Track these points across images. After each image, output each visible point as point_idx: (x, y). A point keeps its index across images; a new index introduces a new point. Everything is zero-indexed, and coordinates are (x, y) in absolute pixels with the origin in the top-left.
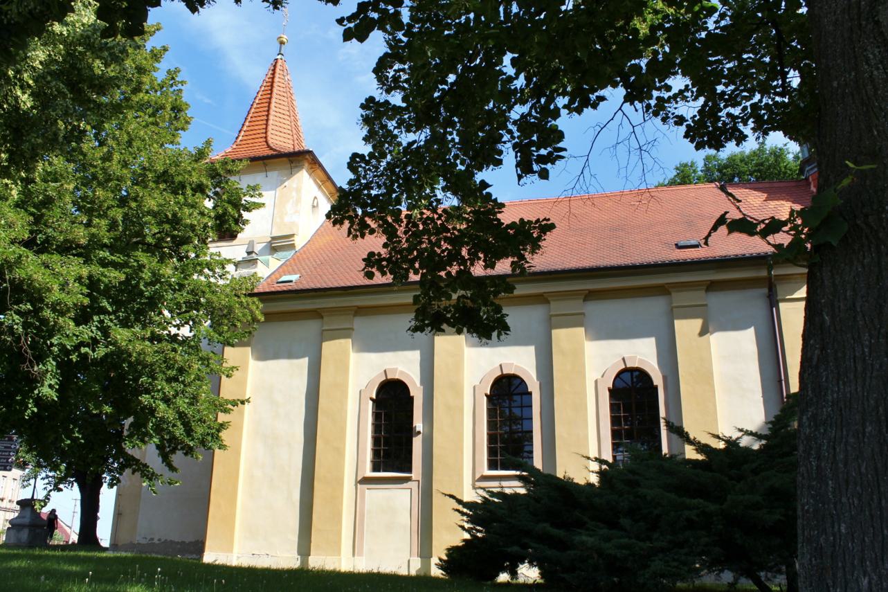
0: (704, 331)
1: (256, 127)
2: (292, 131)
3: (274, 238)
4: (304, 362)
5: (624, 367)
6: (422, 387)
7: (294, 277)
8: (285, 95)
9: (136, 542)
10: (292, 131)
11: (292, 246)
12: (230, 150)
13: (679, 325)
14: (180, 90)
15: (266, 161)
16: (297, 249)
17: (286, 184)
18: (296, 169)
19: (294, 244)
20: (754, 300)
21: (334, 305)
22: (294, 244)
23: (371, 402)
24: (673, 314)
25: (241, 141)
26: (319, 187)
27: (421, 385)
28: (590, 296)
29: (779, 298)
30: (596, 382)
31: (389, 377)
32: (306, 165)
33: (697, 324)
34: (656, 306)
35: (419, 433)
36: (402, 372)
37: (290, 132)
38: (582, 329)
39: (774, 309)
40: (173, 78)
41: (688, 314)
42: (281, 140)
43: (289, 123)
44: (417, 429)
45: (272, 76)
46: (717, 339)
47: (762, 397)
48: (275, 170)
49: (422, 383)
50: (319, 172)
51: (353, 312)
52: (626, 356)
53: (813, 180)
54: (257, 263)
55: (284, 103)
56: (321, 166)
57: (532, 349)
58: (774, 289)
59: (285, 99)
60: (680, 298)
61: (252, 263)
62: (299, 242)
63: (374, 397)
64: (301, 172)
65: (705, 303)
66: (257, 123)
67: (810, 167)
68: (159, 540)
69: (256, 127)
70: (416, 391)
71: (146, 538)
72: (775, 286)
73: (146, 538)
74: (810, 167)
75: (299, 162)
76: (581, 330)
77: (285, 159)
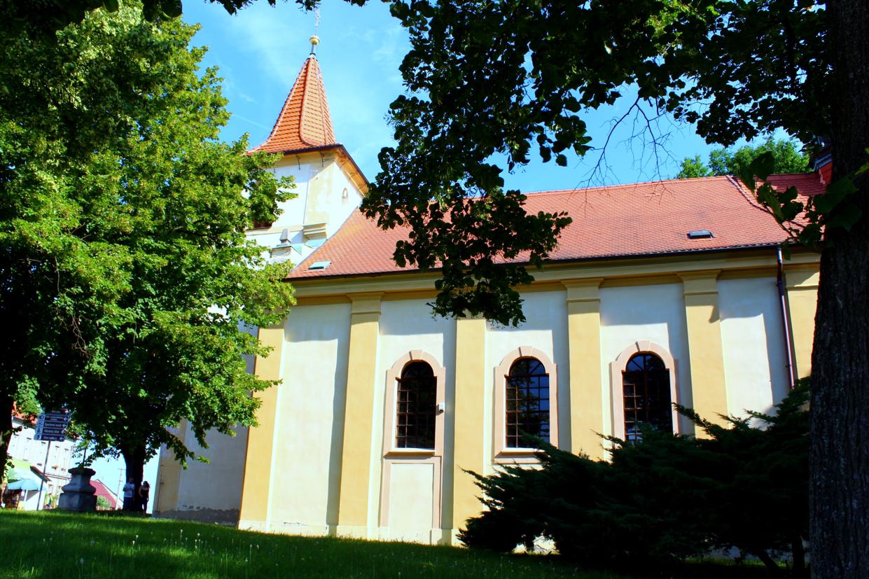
0: (714, 318)
1: (290, 123)
2: (323, 126)
3: (306, 227)
4: (335, 343)
5: (637, 351)
6: (445, 368)
7: (325, 264)
8: (317, 92)
9: (177, 510)
10: (323, 126)
11: (323, 235)
12: (265, 144)
13: (690, 310)
14: (219, 87)
15: (299, 155)
16: (328, 237)
17: (318, 176)
18: (327, 162)
19: (325, 233)
20: (763, 289)
21: (362, 290)
22: (325, 233)
23: (397, 382)
24: (684, 301)
25: (275, 135)
26: (349, 179)
27: (444, 366)
28: (605, 283)
29: (787, 286)
30: (610, 365)
31: (414, 358)
32: (337, 158)
33: (708, 310)
34: (669, 292)
35: (442, 411)
36: (426, 354)
37: (321, 127)
38: (597, 315)
39: (783, 297)
40: (212, 76)
41: (700, 299)
42: (314, 136)
43: (320, 118)
44: (440, 408)
45: (304, 75)
46: (729, 326)
47: (771, 381)
48: (308, 162)
49: (445, 364)
50: (349, 165)
51: (380, 297)
52: (638, 341)
53: (822, 173)
54: (290, 250)
55: (315, 100)
56: (350, 159)
57: (549, 333)
58: (783, 278)
59: (317, 96)
60: (692, 286)
61: (285, 251)
62: (330, 231)
63: (399, 377)
64: (332, 165)
65: (716, 290)
66: (290, 119)
67: (819, 161)
68: (198, 508)
69: (290, 123)
70: (439, 372)
71: (186, 506)
72: (784, 275)
73: (186, 506)
74: (819, 161)
75: (330, 155)
76: (596, 316)
77: (317, 153)
